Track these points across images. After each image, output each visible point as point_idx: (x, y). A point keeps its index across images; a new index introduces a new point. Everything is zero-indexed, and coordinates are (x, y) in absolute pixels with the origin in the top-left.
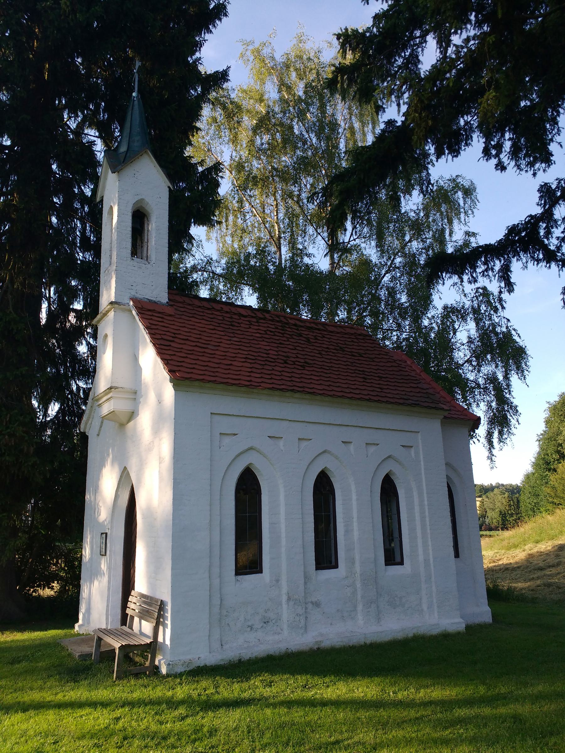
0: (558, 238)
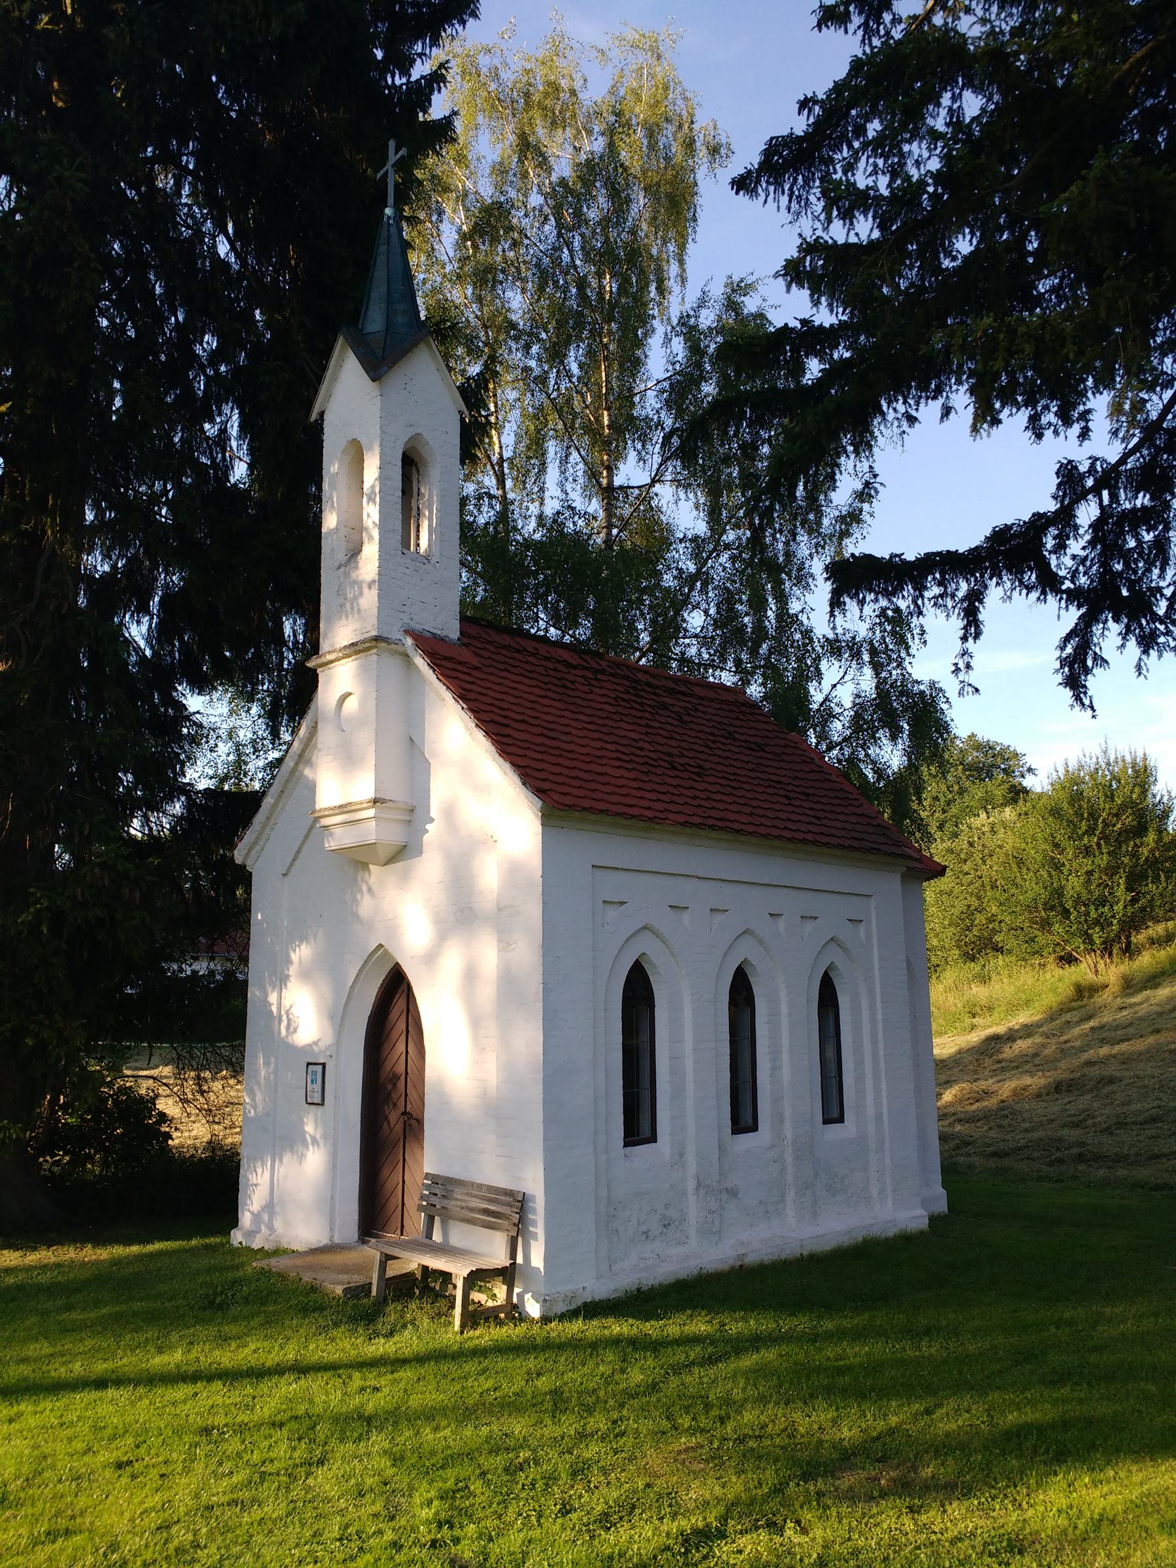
0: (1074, 557)
